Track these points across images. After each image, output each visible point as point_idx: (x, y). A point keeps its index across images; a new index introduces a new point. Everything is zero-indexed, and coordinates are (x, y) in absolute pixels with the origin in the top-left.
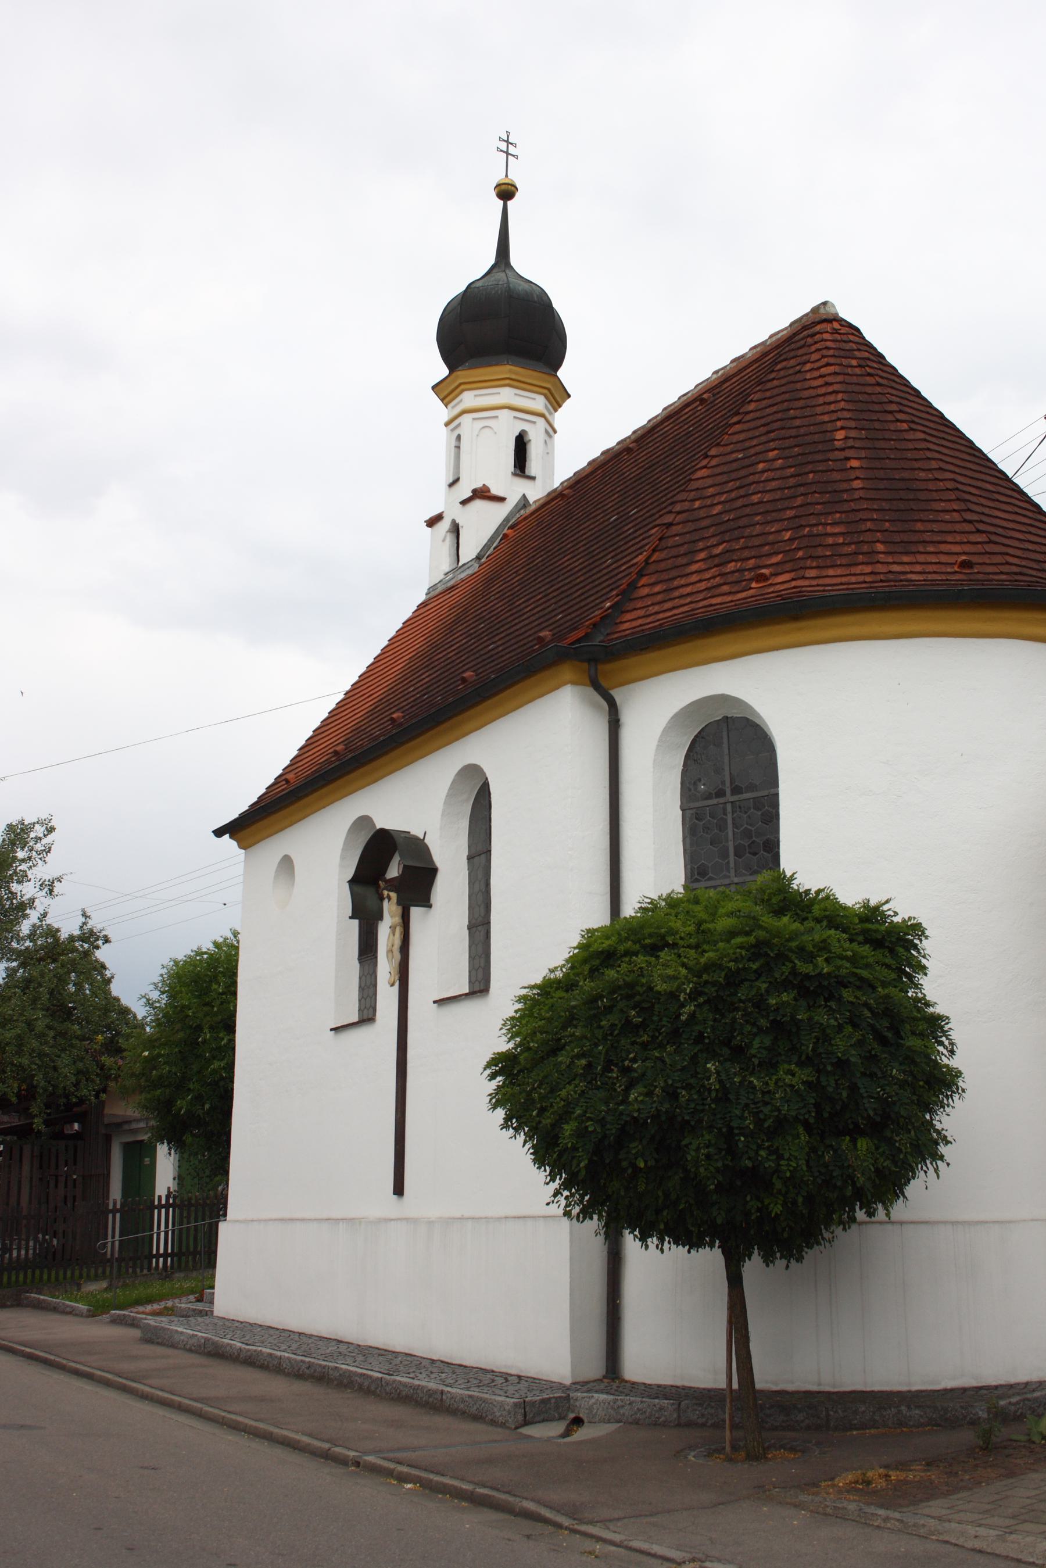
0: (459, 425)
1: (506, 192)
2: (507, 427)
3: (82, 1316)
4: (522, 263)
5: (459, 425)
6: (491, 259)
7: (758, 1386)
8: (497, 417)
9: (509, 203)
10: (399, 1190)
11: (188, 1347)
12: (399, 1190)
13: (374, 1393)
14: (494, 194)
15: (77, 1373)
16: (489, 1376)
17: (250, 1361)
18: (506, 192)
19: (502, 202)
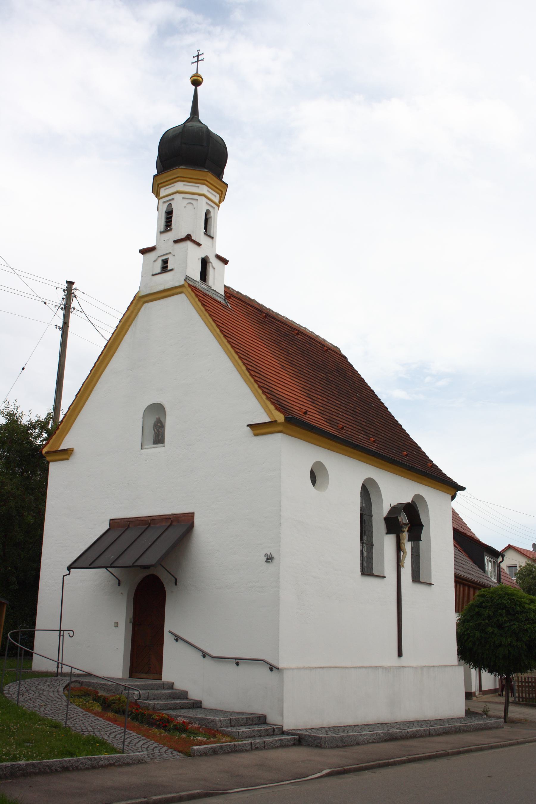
0: (173, 199)
1: (196, 82)
2: (203, 205)
3: (246, 751)
4: (204, 117)
5: (173, 199)
6: (188, 116)
7: (121, 677)
8: (197, 200)
9: (198, 88)
10: (400, 654)
11: (371, 741)
12: (400, 654)
13: (468, 731)
14: (190, 82)
15: (518, 743)
16: (254, 723)
17: (429, 734)
18: (196, 82)
19: (194, 87)
